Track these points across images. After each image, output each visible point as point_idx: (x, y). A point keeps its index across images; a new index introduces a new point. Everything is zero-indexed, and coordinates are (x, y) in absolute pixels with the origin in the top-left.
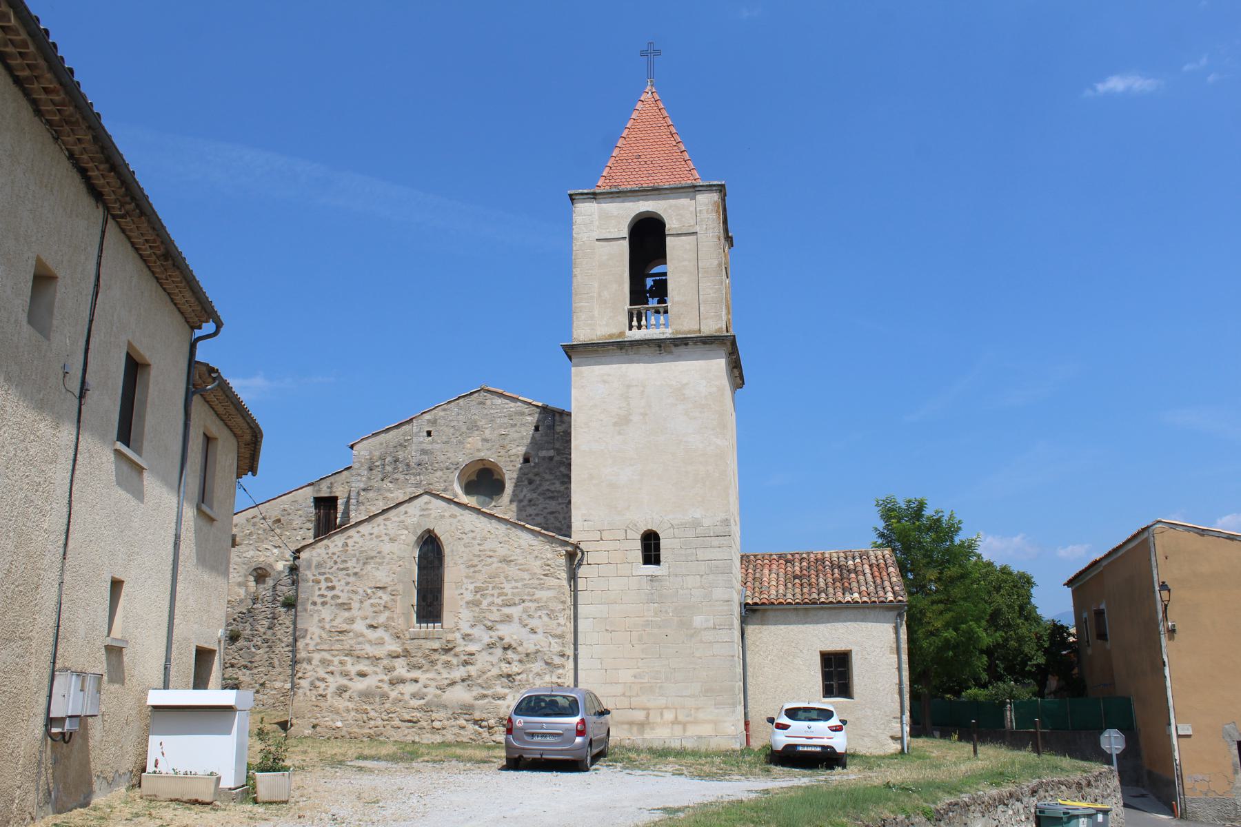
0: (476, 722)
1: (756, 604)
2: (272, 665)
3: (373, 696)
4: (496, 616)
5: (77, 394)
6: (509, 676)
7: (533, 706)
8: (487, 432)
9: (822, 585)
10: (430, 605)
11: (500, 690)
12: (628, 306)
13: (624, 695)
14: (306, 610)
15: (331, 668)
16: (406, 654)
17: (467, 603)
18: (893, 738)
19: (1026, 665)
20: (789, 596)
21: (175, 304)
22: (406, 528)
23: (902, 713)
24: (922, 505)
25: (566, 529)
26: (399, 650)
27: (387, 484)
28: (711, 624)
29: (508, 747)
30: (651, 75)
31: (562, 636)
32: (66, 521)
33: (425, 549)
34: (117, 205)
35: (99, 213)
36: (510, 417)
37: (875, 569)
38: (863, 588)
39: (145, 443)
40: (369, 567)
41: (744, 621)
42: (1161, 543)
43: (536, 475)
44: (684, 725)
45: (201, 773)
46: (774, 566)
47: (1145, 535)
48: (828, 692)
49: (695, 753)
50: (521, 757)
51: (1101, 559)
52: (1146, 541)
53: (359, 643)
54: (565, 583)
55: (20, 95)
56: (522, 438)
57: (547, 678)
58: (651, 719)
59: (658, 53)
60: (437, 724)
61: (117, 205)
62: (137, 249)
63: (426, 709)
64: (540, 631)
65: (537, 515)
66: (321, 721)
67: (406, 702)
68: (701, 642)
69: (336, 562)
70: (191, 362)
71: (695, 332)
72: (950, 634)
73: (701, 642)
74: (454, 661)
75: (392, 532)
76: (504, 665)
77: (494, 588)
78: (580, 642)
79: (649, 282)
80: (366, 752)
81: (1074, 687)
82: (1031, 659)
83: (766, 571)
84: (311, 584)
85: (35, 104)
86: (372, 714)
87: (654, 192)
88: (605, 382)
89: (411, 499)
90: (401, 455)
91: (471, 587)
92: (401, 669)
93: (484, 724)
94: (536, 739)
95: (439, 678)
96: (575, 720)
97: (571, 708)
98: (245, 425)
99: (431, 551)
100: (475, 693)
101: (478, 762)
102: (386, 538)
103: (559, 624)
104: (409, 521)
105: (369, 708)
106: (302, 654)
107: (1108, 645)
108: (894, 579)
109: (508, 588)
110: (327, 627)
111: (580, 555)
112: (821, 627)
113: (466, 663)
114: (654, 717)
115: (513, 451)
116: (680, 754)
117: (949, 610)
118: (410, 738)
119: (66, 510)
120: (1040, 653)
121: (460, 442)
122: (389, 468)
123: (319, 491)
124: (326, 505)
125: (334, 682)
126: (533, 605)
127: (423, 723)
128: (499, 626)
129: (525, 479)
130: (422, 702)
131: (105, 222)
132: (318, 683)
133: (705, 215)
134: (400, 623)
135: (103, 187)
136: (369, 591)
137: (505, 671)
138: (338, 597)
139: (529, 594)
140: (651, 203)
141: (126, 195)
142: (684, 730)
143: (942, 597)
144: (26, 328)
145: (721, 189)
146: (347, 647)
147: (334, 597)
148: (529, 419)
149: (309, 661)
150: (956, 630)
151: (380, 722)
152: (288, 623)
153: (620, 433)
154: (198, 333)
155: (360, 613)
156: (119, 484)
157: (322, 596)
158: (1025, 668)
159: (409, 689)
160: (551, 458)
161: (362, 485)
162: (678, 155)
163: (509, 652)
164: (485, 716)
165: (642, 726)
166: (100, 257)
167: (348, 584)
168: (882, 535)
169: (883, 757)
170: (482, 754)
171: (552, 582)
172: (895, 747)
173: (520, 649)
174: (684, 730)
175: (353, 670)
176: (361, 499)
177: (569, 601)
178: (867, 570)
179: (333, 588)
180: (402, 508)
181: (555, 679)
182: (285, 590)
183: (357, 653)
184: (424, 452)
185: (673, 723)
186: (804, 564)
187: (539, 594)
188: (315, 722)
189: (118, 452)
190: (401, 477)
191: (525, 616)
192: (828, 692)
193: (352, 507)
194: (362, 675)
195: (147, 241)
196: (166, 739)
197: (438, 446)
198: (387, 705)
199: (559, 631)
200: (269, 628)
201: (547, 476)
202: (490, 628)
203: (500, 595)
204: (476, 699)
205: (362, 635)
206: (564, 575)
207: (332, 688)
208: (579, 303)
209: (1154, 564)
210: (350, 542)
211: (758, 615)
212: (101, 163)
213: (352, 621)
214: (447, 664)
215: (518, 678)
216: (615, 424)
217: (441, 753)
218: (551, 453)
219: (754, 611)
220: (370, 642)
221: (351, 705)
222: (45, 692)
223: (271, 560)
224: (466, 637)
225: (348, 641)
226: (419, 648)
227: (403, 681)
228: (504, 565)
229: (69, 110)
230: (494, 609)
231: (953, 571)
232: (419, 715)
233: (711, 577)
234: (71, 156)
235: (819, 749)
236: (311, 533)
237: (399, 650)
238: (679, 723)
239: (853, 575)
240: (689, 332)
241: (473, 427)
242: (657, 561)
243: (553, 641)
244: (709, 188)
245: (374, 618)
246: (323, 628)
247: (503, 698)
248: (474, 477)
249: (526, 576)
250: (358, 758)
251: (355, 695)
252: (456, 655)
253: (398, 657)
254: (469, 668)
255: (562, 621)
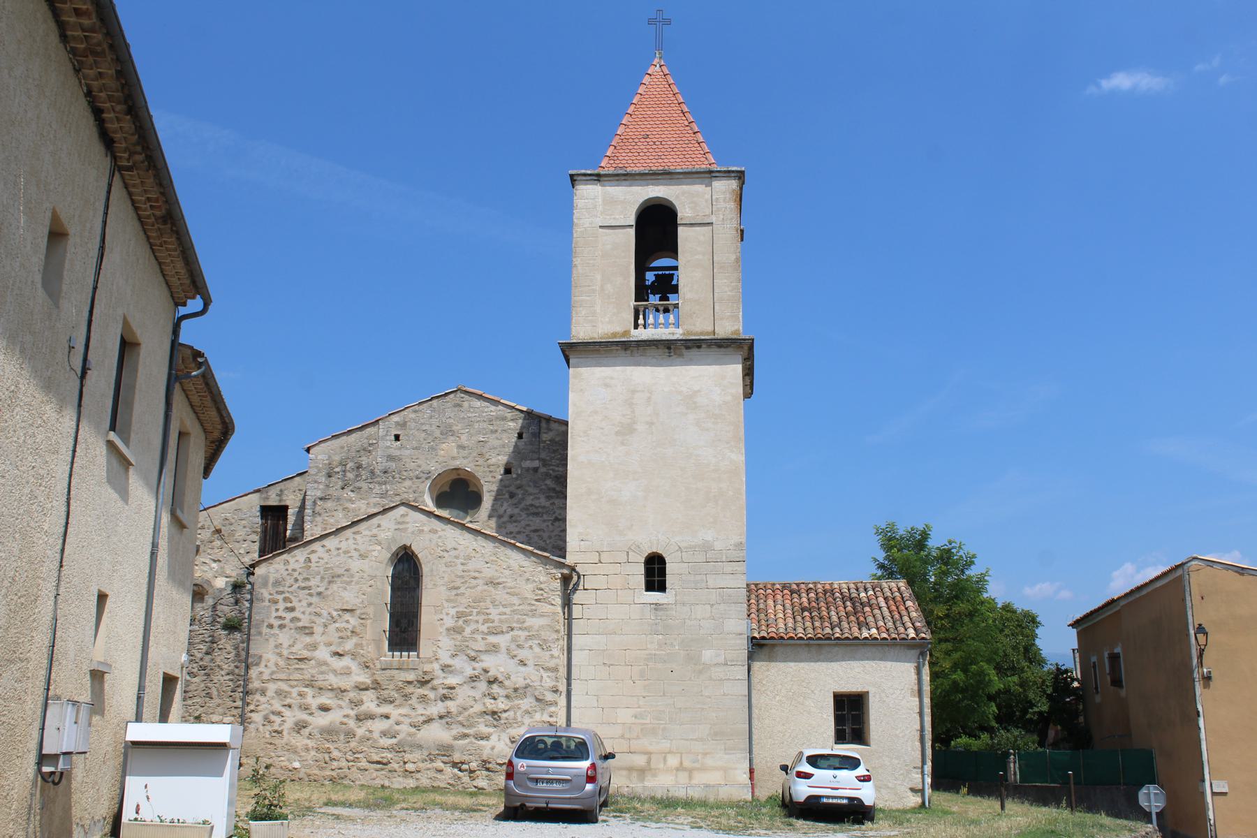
0: (455, 765)
1: (763, 638)
2: (209, 696)
3: (337, 733)
4: (480, 645)
5: (79, 373)
6: (494, 713)
7: (530, 748)
8: (464, 437)
9: (835, 618)
10: (404, 631)
11: (484, 729)
12: (633, 303)
13: (622, 737)
14: (260, 633)
15: (288, 701)
16: (376, 686)
17: (448, 630)
18: (912, 790)
19: (1027, 712)
20: (800, 630)
21: (164, 276)
22: (379, 544)
23: (924, 762)
24: (925, 535)
25: (562, 551)
26: (368, 681)
27: (348, 494)
28: (721, 660)
29: (507, 792)
30: (660, 47)
31: (555, 670)
32: (63, 522)
33: (400, 567)
34: (126, 155)
35: (107, 163)
36: (490, 421)
37: (891, 602)
38: (881, 623)
39: (132, 435)
40: (334, 587)
41: (751, 657)
42: (1197, 582)
43: (519, 487)
44: (690, 771)
45: (190, 821)
46: (779, 597)
47: (1179, 572)
48: (840, 738)
49: (704, 804)
50: (523, 805)
51: (1119, 599)
52: (1180, 579)
53: (322, 673)
54: (559, 609)
55: (49, 14)
56: (504, 446)
57: (538, 716)
58: (653, 766)
59: (668, 22)
60: (410, 767)
61: (126, 155)
62: (136, 209)
63: (398, 749)
64: (530, 663)
65: (519, 533)
66: (275, 761)
67: (375, 741)
68: (711, 679)
69: (296, 580)
70: (175, 345)
71: (708, 333)
72: (958, 676)
73: (711, 679)
74: (432, 695)
75: (362, 548)
76: (488, 701)
77: (478, 613)
78: (574, 675)
79: (650, 277)
80: (334, 797)
81: (1079, 738)
82: (1032, 705)
83: (770, 602)
84: (267, 603)
85: (62, 27)
86: (336, 754)
87: (666, 176)
88: (607, 385)
89: (385, 511)
90: (364, 461)
91: (453, 612)
92: (370, 703)
93: (464, 767)
94: (540, 785)
95: (413, 713)
96: (585, 764)
97: (580, 750)
98: (218, 419)
99: (407, 568)
100: (454, 732)
101: (464, 810)
102: (355, 554)
103: (552, 656)
104: (382, 536)
105: (331, 746)
106: (256, 684)
107: (1123, 693)
108: (914, 614)
109: (494, 613)
110: (285, 653)
111: (575, 578)
112: (835, 665)
113: (445, 698)
114: (657, 763)
115: (493, 461)
116: (688, 804)
117: (956, 650)
118: (378, 782)
119: (64, 509)
120: (1044, 700)
121: (432, 448)
122: (350, 475)
123: (267, 498)
124: (274, 515)
125: (291, 717)
126: (523, 634)
127: (396, 766)
128: (483, 657)
129: (506, 492)
130: (394, 741)
131: (112, 176)
132: (273, 718)
133: (722, 205)
134: (369, 651)
135: (115, 132)
136: (335, 614)
137: (490, 707)
138: (299, 620)
139: (518, 622)
140: (657, 188)
141: (138, 143)
142: (690, 778)
143: (950, 635)
144: (40, 292)
145: (740, 176)
146: (308, 676)
147: (293, 620)
148: (512, 424)
149: (263, 692)
150: (965, 671)
151: (344, 764)
152: (229, 648)
153: (623, 444)
154: (183, 311)
155: (324, 638)
156: (109, 481)
157: (280, 617)
158: (1060, 716)
159: (378, 726)
160: (536, 470)
161: (319, 494)
162: (690, 136)
163: (495, 686)
164: (466, 758)
165: (642, 772)
166: (106, 214)
167: (310, 604)
168: (881, 566)
169: (905, 811)
170: (468, 801)
171: (545, 608)
172: (915, 800)
173: (507, 683)
174: (690, 778)
175: (314, 703)
176: (318, 508)
177: (562, 629)
178: (883, 604)
179: (292, 609)
180: (375, 521)
181: (546, 718)
182: (227, 611)
183: (319, 684)
184: (391, 458)
185: (677, 770)
186: (812, 595)
187: (530, 621)
188: (269, 762)
189: (110, 444)
190: (364, 485)
191: (513, 646)
192: (840, 738)
193: (307, 518)
194: (325, 709)
195: (149, 199)
196: (153, 781)
197: (408, 452)
198: (353, 744)
199: (552, 664)
200: (207, 653)
201: (531, 490)
202: (474, 659)
203: (485, 621)
204: (455, 739)
205: (325, 663)
206: (559, 601)
207: (289, 723)
208: (578, 297)
209: (1189, 604)
210: (314, 557)
211: (766, 650)
212: (119, 103)
213: (314, 647)
214: (423, 699)
215: (504, 715)
216: (617, 433)
217: (418, 799)
218: (536, 464)
219: (761, 646)
220: (335, 672)
221: (311, 743)
222: (37, 725)
223: (209, 575)
224: (446, 668)
225: (310, 670)
226: (391, 679)
227: (371, 717)
228: (491, 588)
229: (97, 37)
230: (479, 637)
231: (962, 607)
232: (389, 756)
233: (722, 607)
234: (89, 94)
235: (845, 801)
236: (256, 547)
237: (368, 681)
238: (685, 769)
239: (867, 609)
240: (702, 334)
241: (448, 432)
242: (662, 588)
243: (545, 675)
244: (728, 174)
245: (340, 644)
246: (280, 655)
247: (487, 738)
248: (447, 489)
249: (515, 600)
250: (326, 804)
251: (315, 732)
252: (434, 689)
253: (366, 689)
254: (449, 703)
255: (556, 652)
